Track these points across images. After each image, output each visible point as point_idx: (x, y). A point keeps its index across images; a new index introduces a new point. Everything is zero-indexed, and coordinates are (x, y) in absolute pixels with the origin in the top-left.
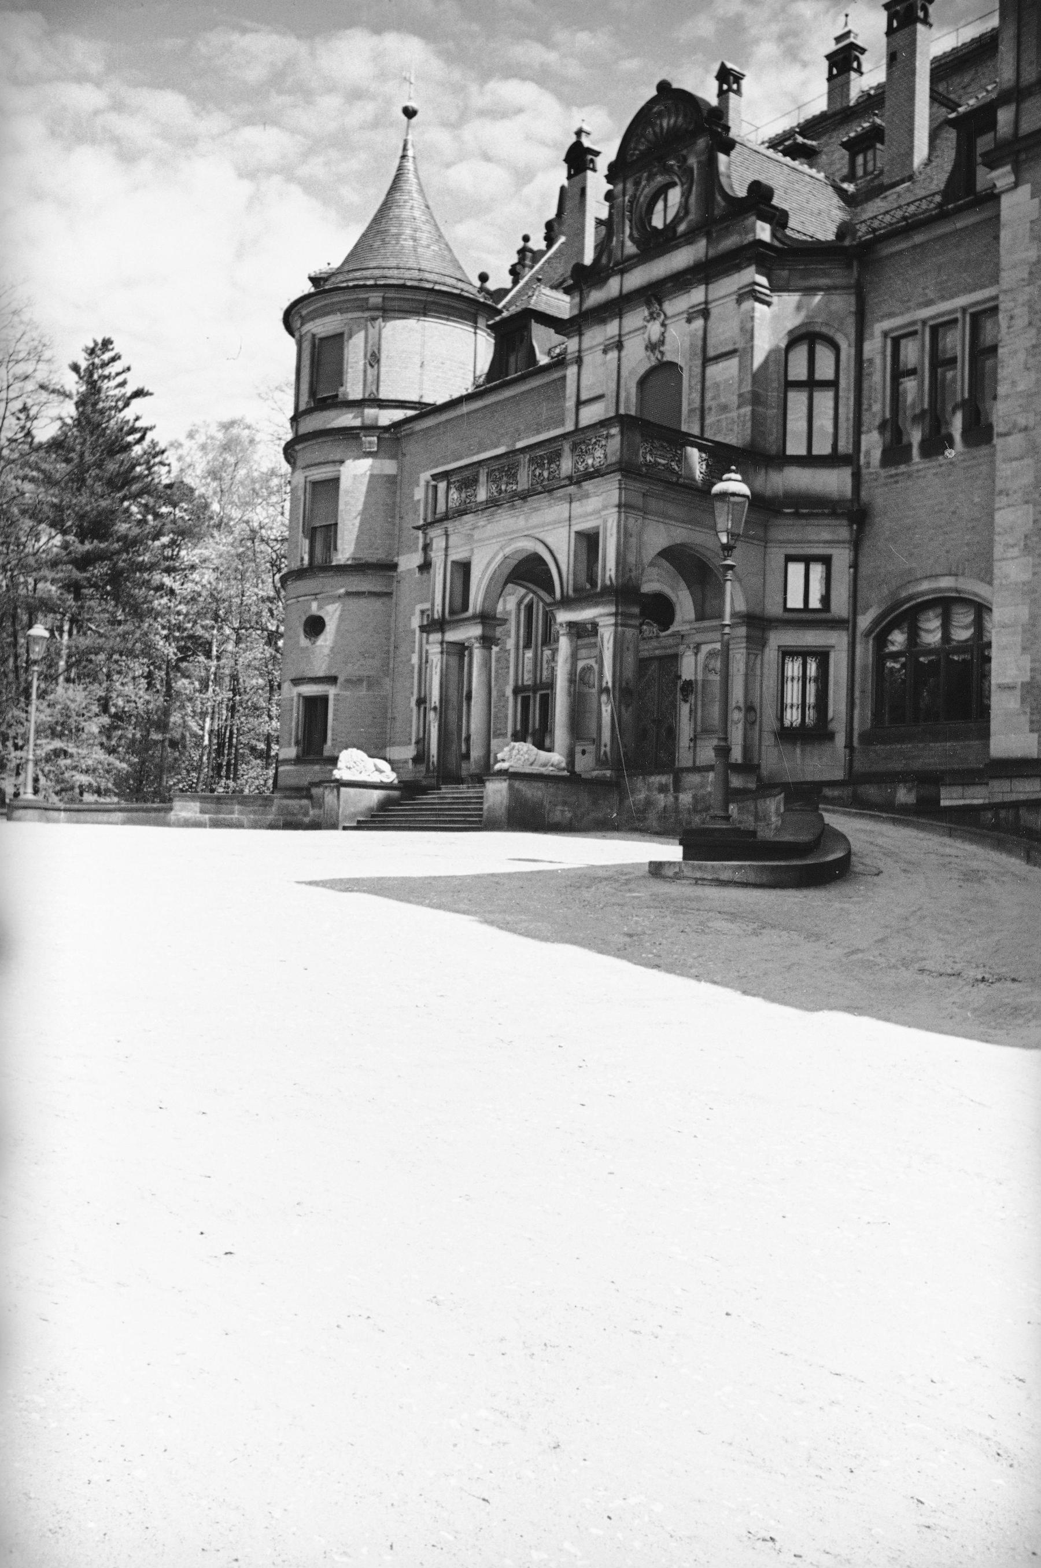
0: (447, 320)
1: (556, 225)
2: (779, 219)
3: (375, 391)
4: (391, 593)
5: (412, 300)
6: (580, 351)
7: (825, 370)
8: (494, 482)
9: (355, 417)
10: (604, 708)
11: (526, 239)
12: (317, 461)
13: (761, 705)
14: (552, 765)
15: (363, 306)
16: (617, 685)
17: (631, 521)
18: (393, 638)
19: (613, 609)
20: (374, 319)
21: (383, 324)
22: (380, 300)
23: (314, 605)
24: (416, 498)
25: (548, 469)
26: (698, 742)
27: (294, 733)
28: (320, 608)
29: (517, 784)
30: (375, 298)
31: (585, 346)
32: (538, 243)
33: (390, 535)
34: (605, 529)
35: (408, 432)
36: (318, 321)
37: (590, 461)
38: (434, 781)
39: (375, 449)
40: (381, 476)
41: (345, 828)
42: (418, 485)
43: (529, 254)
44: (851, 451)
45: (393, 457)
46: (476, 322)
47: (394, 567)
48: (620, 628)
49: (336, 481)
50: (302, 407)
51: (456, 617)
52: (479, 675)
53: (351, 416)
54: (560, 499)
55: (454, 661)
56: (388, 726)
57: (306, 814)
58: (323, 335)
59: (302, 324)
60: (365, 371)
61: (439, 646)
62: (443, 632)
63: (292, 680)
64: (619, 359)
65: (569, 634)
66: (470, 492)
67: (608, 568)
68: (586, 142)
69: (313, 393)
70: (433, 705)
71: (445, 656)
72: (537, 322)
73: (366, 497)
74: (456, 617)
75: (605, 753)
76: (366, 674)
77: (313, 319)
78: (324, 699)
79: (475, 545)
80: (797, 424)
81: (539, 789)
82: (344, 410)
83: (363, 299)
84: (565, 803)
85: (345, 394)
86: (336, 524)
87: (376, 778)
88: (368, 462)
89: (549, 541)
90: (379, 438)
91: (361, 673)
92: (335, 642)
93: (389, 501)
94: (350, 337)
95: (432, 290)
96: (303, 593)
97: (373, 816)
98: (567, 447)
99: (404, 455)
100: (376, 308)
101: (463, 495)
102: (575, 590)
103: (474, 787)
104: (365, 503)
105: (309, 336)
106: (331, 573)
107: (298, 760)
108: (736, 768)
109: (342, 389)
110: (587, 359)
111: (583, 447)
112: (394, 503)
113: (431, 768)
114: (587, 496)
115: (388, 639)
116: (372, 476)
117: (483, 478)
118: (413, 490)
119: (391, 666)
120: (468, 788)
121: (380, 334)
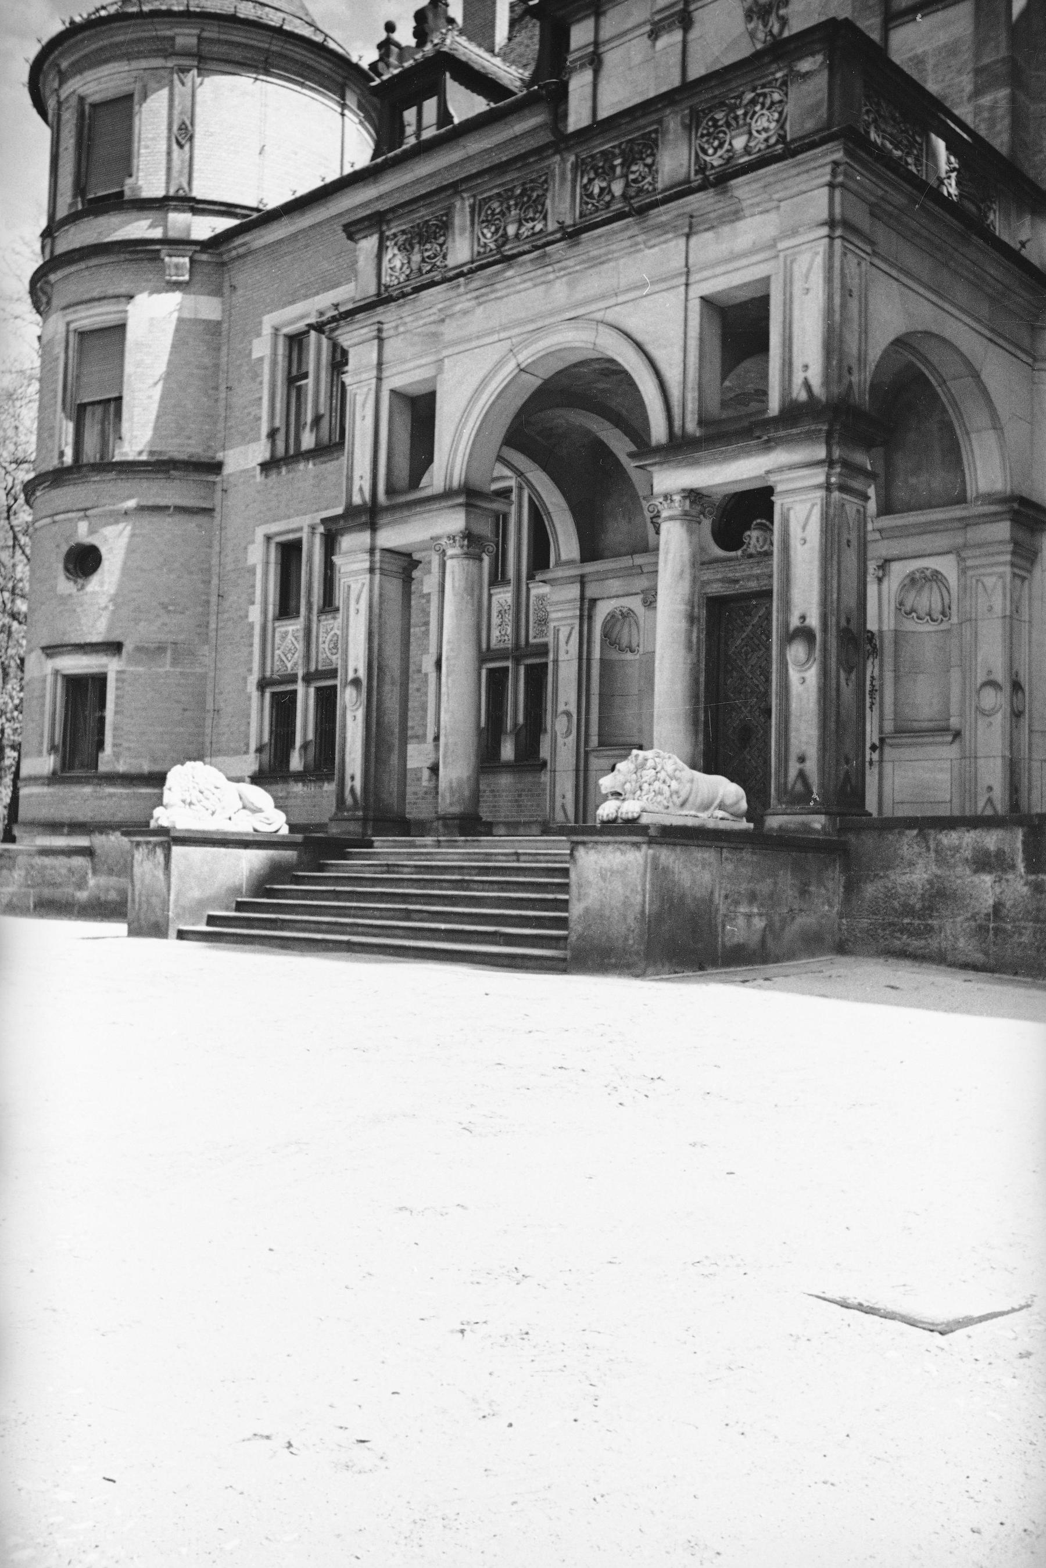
0: (302, 85)
1: (430, 16)
3: (185, 185)
4: (212, 510)
5: (246, 46)
6: (596, 43)
8: (488, 222)
9: (151, 226)
10: (794, 675)
11: (390, 27)
12: (87, 296)
13: (1030, 680)
14: (721, 807)
15: (166, 49)
16: (832, 620)
17: (852, 260)
18: (215, 581)
19: (821, 453)
20: (184, 70)
21: (198, 80)
22: (194, 41)
23: (83, 527)
24: (255, 355)
25: (625, 176)
26: (887, 750)
27: (46, 734)
28: (92, 531)
29: (667, 856)
30: (186, 37)
31: (604, 35)
33: (211, 417)
34: (788, 282)
35: (241, 250)
36: (90, 75)
37: (739, 143)
38: (354, 828)
39: (186, 278)
40: (197, 321)
41: (182, 935)
42: (259, 335)
43: (395, 50)
44: (654, 443)
45: (217, 292)
46: (343, 97)
47: (216, 467)
48: (836, 494)
49: (121, 328)
50: (62, 213)
51: (402, 499)
52: (459, 613)
53: (145, 223)
54: (663, 228)
55: (394, 587)
56: (208, 722)
57: (81, 885)
58: (96, 98)
59: (61, 84)
60: (169, 153)
61: (367, 556)
62: (374, 528)
63: (43, 649)
64: (685, 43)
65: (686, 517)
66: (431, 248)
67: (798, 363)
69: (80, 188)
70: (351, 675)
71: (377, 577)
72: (454, 78)
73: (171, 353)
74: (402, 499)
75: (802, 775)
76: (171, 638)
77: (80, 72)
78: (100, 680)
79: (445, 353)
81: (704, 865)
82: (135, 214)
83: (165, 38)
84: (752, 897)
85: (136, 189)
86: (119, 399)
87: (243, 825)
88: (175, 298)
89: (633, 323)
90: (192, 261)
91: (162, 637)
92: (121, 585)
93: (206, 361)
94: (145, 97)
95: (279, 31)
96: (62, 508)
97: (240, 906)
98: (673, 123)
99: (233, 288)
100: (186, 54)
101: (416, 258)
102: (701, 423)
103: (452, 844)
104: (170, 362)
105: (74, 101)
106: (112, 475)
107: (54, 779)
109: (129, 181)
110: (611, 58)
111: (719, 116)
112: (217, 366)
113: (349, 800)
114: (737, 215)
115: (208, 582)
116: (181, 321)
117: (461, 218)
118: (250, 342)
119: (213, 626)
120: (438, 844)
121: (193, 96)
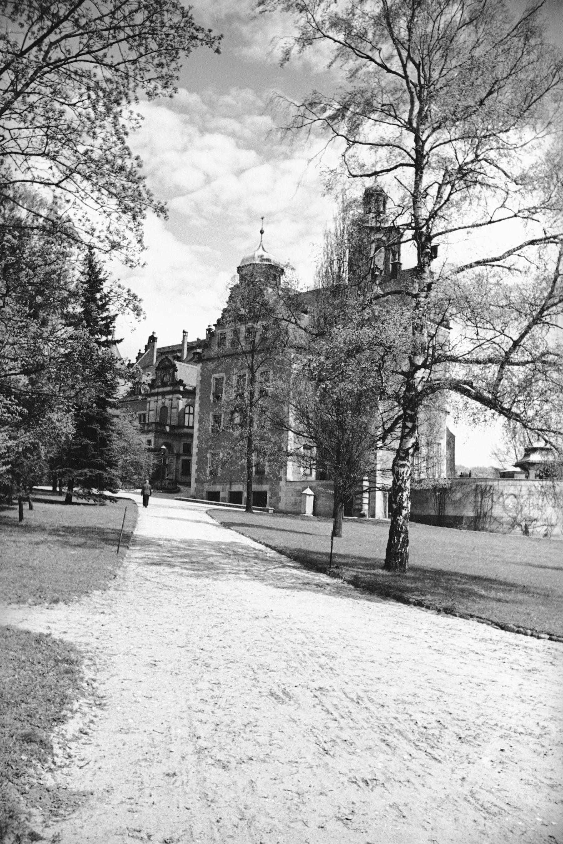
2: (184, 386)
7: (192, 411)
32: (143, 351)
68: (155, 336)
80: (186, 420)
108: (54, 489)
